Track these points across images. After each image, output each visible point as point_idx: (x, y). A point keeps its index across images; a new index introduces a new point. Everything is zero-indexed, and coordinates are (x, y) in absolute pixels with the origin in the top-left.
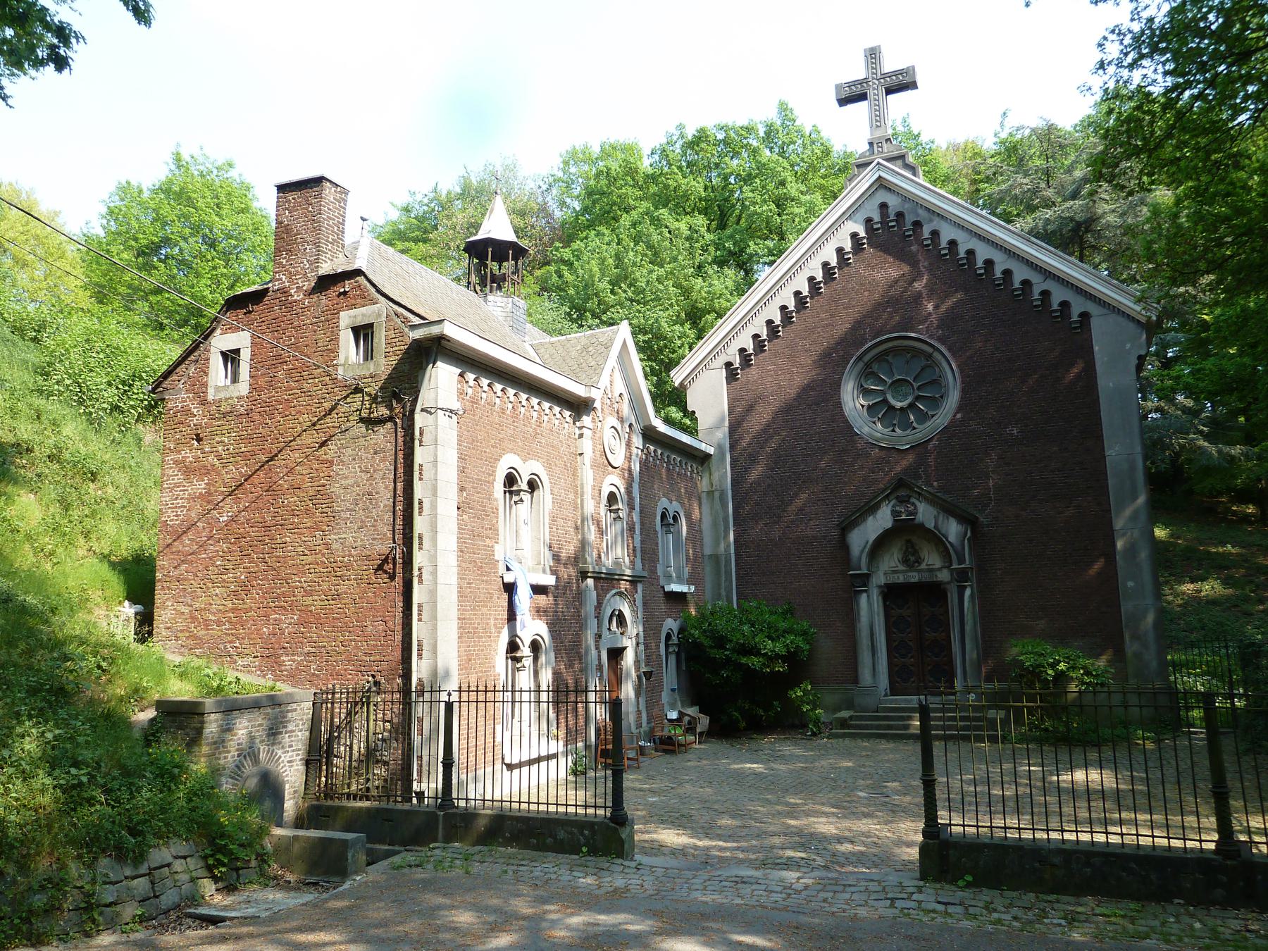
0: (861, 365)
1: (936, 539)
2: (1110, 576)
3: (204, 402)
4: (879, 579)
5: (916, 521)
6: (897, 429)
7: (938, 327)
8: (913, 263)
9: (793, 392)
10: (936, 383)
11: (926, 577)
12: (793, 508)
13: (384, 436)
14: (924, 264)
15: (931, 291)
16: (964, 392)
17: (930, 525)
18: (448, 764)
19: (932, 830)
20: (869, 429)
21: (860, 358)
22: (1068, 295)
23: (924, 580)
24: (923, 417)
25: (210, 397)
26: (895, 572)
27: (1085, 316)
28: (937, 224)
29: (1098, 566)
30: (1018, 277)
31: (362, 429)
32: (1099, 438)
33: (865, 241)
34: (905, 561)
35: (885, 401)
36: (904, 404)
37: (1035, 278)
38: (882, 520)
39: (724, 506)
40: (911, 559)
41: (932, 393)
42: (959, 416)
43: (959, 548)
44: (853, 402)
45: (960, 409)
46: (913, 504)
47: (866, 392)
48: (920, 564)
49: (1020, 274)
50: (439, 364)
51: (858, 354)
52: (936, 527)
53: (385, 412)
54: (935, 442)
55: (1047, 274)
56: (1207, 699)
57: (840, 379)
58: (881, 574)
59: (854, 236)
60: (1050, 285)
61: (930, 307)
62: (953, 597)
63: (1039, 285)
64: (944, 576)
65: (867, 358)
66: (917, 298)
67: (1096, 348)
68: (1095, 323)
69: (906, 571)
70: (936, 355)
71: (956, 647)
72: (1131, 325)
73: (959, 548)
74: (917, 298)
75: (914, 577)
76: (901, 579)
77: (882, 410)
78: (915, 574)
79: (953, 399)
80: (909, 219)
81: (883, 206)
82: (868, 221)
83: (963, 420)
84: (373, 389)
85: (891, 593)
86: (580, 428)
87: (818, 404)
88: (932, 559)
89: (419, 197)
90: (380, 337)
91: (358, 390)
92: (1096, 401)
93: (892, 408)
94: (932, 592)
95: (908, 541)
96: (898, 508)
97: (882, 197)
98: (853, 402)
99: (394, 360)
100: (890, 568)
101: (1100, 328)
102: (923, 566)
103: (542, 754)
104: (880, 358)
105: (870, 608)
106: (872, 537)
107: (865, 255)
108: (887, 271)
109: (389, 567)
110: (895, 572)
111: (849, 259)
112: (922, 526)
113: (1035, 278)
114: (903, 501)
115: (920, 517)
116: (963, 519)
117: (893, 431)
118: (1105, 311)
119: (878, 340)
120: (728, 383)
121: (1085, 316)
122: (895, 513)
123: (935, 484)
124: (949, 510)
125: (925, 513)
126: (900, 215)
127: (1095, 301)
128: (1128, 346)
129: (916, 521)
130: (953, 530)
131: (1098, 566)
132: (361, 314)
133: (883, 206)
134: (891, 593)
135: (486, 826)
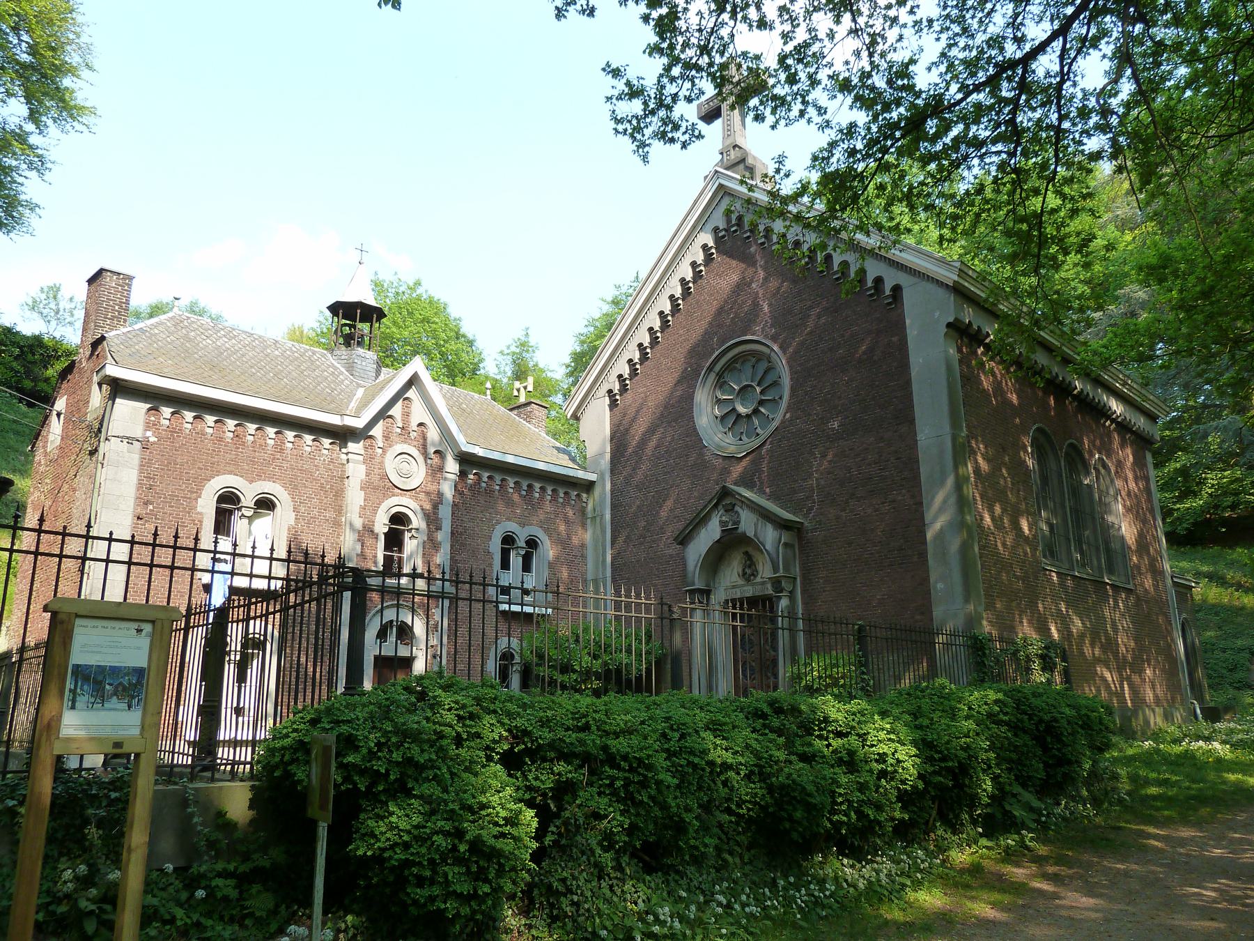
0: (712, 376)
5: (740, 531)
6: (744, 437)
7: (772, 326)
21: (710, 369)
23: (757, 594)
26: (734, 587)
27: (897, 289)
32: (912, 421)
33: (713, 251)
35: (734, 410)
39: (603, 532)
42: (788, 415)
43: (774, 555)
46: (737, 512)
48: (755, 576)
50: (118, 400)
51: (708, 364)
52: (755, 535)
54: (767, 446)
57: (694, 392)
58: (722, 589)
59: (705, 247)
65: (718, 368)
67: (908, 322)
68: (906, 295)
69: (743, 586)
70: (773, 354)
72: (941, 292)
73: (774, 555)
77: (731, 420)
78: (750, 588)
82: (716, 230)
83: (791, 420)
86: (347, 454)
87: (675, 420)
89: (624, 289)
92: (908, 383)
93: (739, 416)
95: (746, 553)
96: (724, 518)
97: (726, 201)
102: (758, 579)
103: (239, 738)
104: (729, 367)
107: (714, 265)
108: (728, 275)
110: (734, 587)
111: (701, 271)
117: (741, 440)
118: (915, 280)
119: (723, 348)
120: (611, 410)
121: (897, 289)
122: (722, 523)
123: (768, 490)
127: (906, 272)
128: (937, 314)
129: (740, 531)
135: (253, 804)
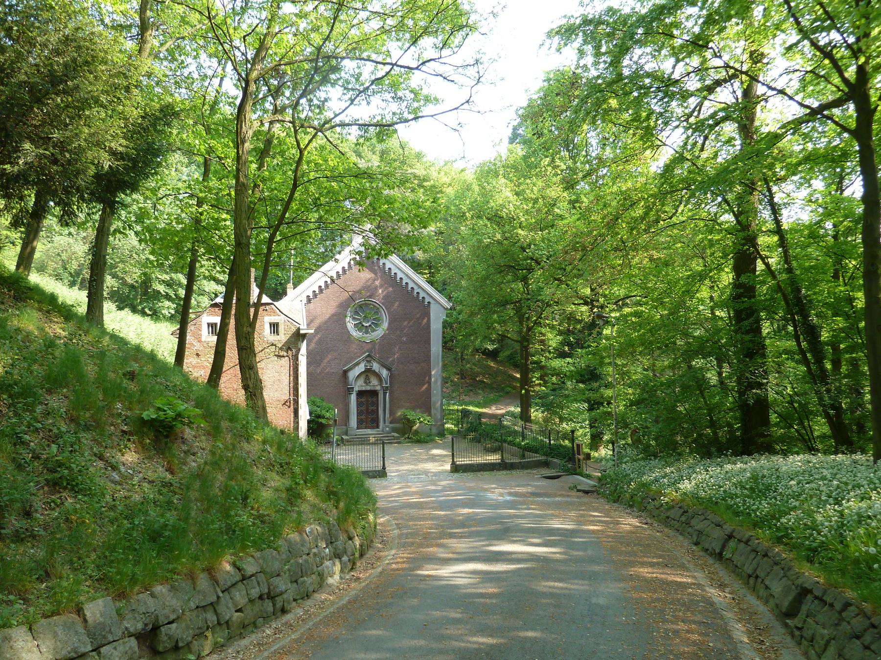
1: (378, 376)
2: (429, 389)
3: (200, 341)
4: (356, 389)
8: (376, 274)
9: (328, 316)
11: (372, 388)
12: (325, 361)
13: (285, 362)
14: (379, 274)
15: (381, 286)
17: (377, 371)
19: (453, 463)
20: (355, 334)
24: (374, 331)
25: (203, 340)
29: (426, 386)
30: (427, 301)
31: (276, 358)
32: (430, 344)
34: (365, 382)
37: (415, 287)
38: (361, 368)
40: (367, 381)
41: (376, 324)
44: (350, 324)
47: (354, 319)
49: (411, 285)
53: (285, 354)
55: (420, 287)
60: (419, 290)
61: (380, 291)
62: (381, 396)
64: (378, 388)
66: (376, 288)
68: (432, 306)
74: (376, 288)
75: (368, 388)
77: (359, 326)
79: (385, 325)
84: (280, 345)
85: (360, 394)
88: (374, 381)
90: (281, 329)
91: (273, 345)
98: (350, 324)
99: (288, 337)
100: (359, 385)
101: (433, 307)
105: (353, 397)
109: (288, 404)
112: (374, 371)
113: (415, 287)
114: (369, 362)
116: (389, 369)
122: (366, 366)
124: (384, 366)
125: (376, 366)
130: (384, 373)
131: (426, 386)
132: (274, 319)
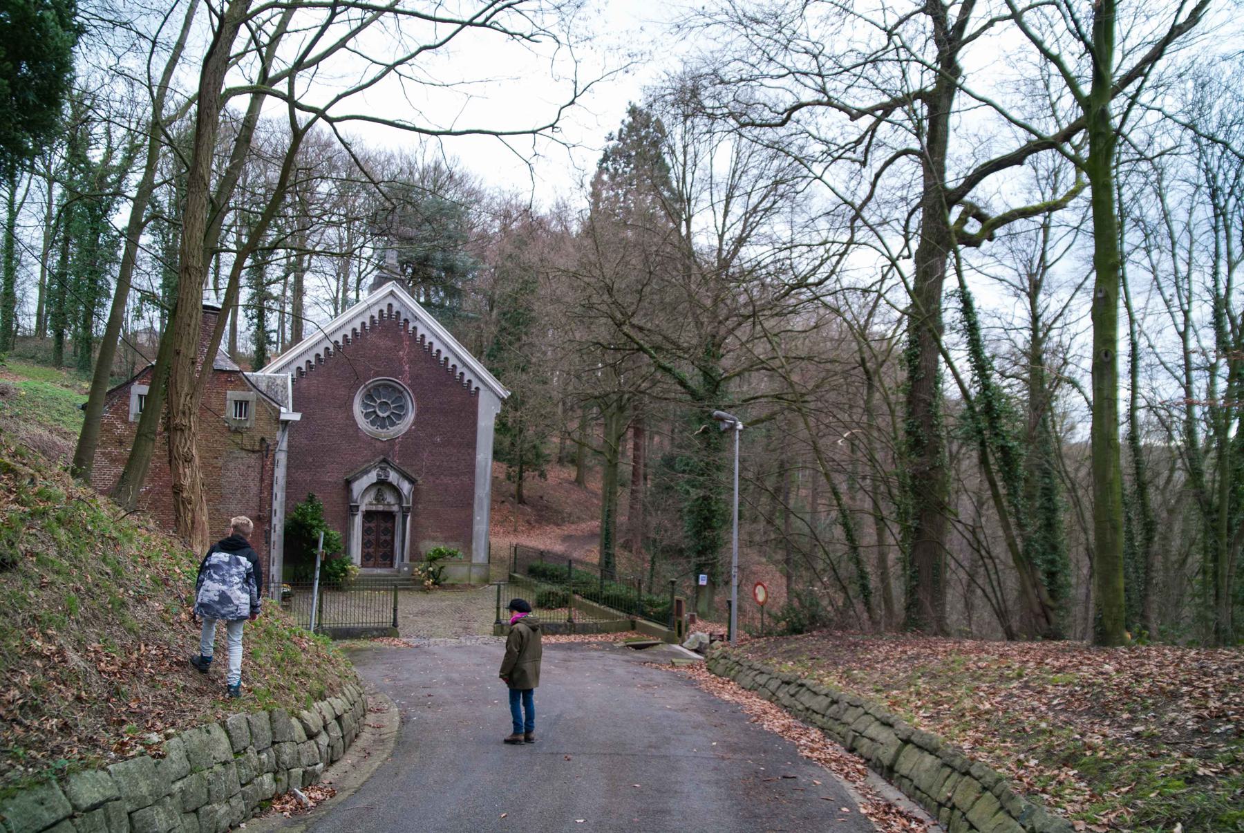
1: (396, 490)
4: (363, 508)
10: (402, 407)
11: (387, 509)
16: (417, 416)
18: (498, 608)
22: (471, 377)
24: (393, 424)
28: (417, 324)
30: (474, 384)
32: (474, 449)
34: (376, 499)
36: (385, 415)
45: (414, 424)
55: (465, 364)
56: (1220, 669)
60: (465, 370)
62: (399, 519)
63: (460, 369)
64: (395, 508)
68: (481, 393)
71: (397, 544)
75: (381, 508)
76: (374, 508)
77: (376, 420)
79: (411, 416)
80: (403, 317)
81: (390, 305)
85: (368, 515)
88: (390, 498)
92: (474, 433)
94: (389, 516)
97: (390, 300)
100: (366, 503)
106: (365, 486)
113: (459, 365)
115: (390, 479)
121: (477, 389)
122: (378, 475)
125: (393, 477)
126: (398, 313)
133: (390, 305)
134: (368, 515)
